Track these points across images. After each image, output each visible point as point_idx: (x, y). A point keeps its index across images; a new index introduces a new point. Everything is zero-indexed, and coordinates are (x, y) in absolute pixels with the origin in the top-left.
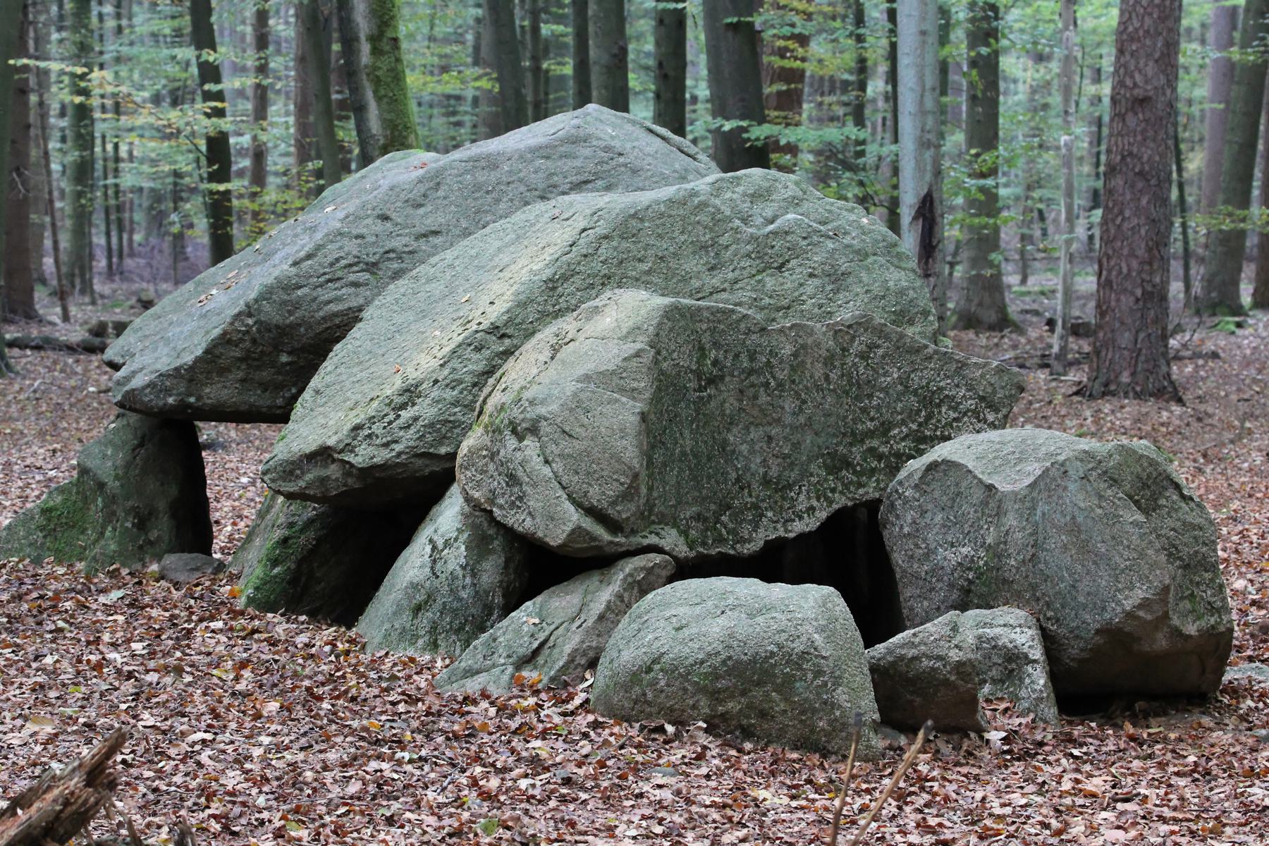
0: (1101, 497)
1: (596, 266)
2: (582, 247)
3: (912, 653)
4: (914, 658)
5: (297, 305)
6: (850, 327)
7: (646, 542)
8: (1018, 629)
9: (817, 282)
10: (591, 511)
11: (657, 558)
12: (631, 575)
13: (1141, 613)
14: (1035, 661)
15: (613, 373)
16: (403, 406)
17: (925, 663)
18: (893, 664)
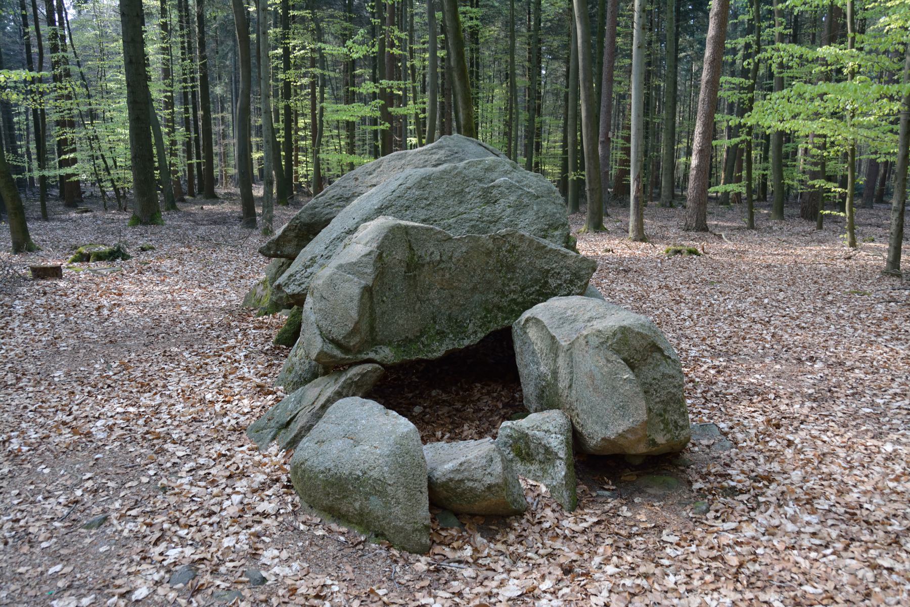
0: (608, 361)
1: (402, 202)
2: (396, 194)
3: (458, 477)
4: (462, 481)
5: (315, 215)
6: (503, 236)
7: (366, 357)
8: (554, 435)
9: (511, 209)
10: (333, 341)
11: (369, 367)
12: (350, 378)
13: (629, 436)
14: (561, 459)
15: (355, 264)
16: (309, 266)
17: (471, 484)
18: (447, 482)
